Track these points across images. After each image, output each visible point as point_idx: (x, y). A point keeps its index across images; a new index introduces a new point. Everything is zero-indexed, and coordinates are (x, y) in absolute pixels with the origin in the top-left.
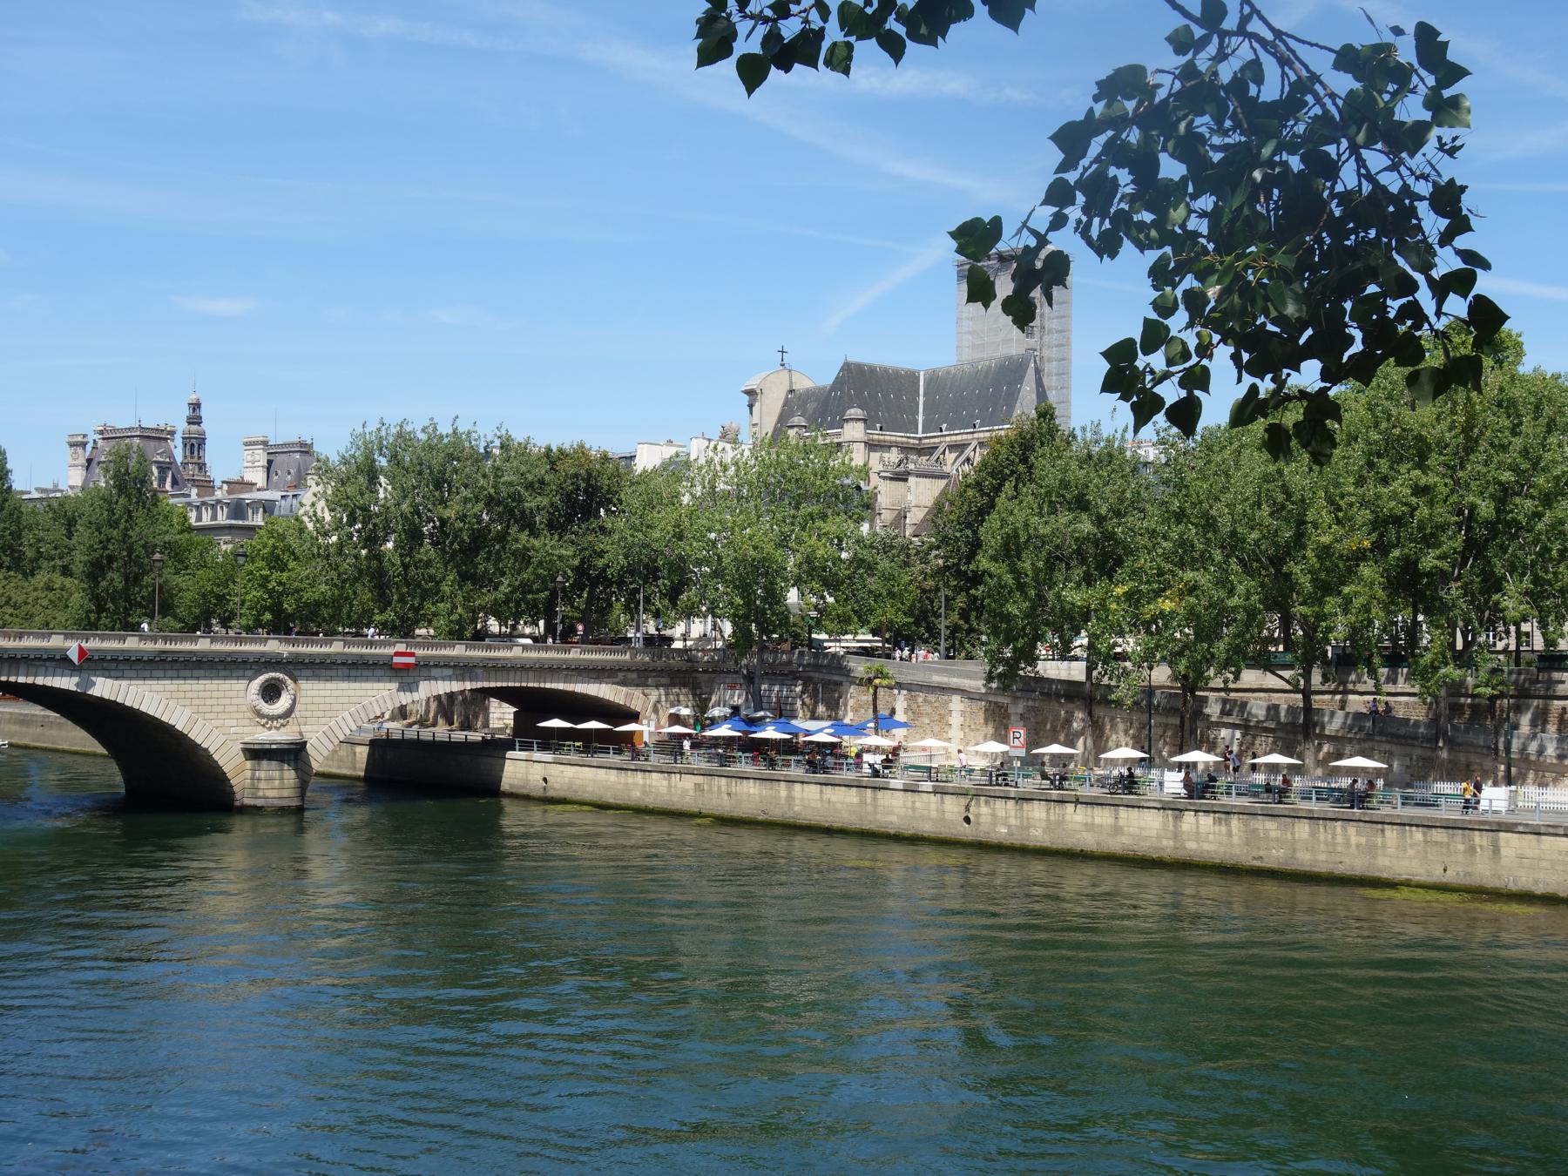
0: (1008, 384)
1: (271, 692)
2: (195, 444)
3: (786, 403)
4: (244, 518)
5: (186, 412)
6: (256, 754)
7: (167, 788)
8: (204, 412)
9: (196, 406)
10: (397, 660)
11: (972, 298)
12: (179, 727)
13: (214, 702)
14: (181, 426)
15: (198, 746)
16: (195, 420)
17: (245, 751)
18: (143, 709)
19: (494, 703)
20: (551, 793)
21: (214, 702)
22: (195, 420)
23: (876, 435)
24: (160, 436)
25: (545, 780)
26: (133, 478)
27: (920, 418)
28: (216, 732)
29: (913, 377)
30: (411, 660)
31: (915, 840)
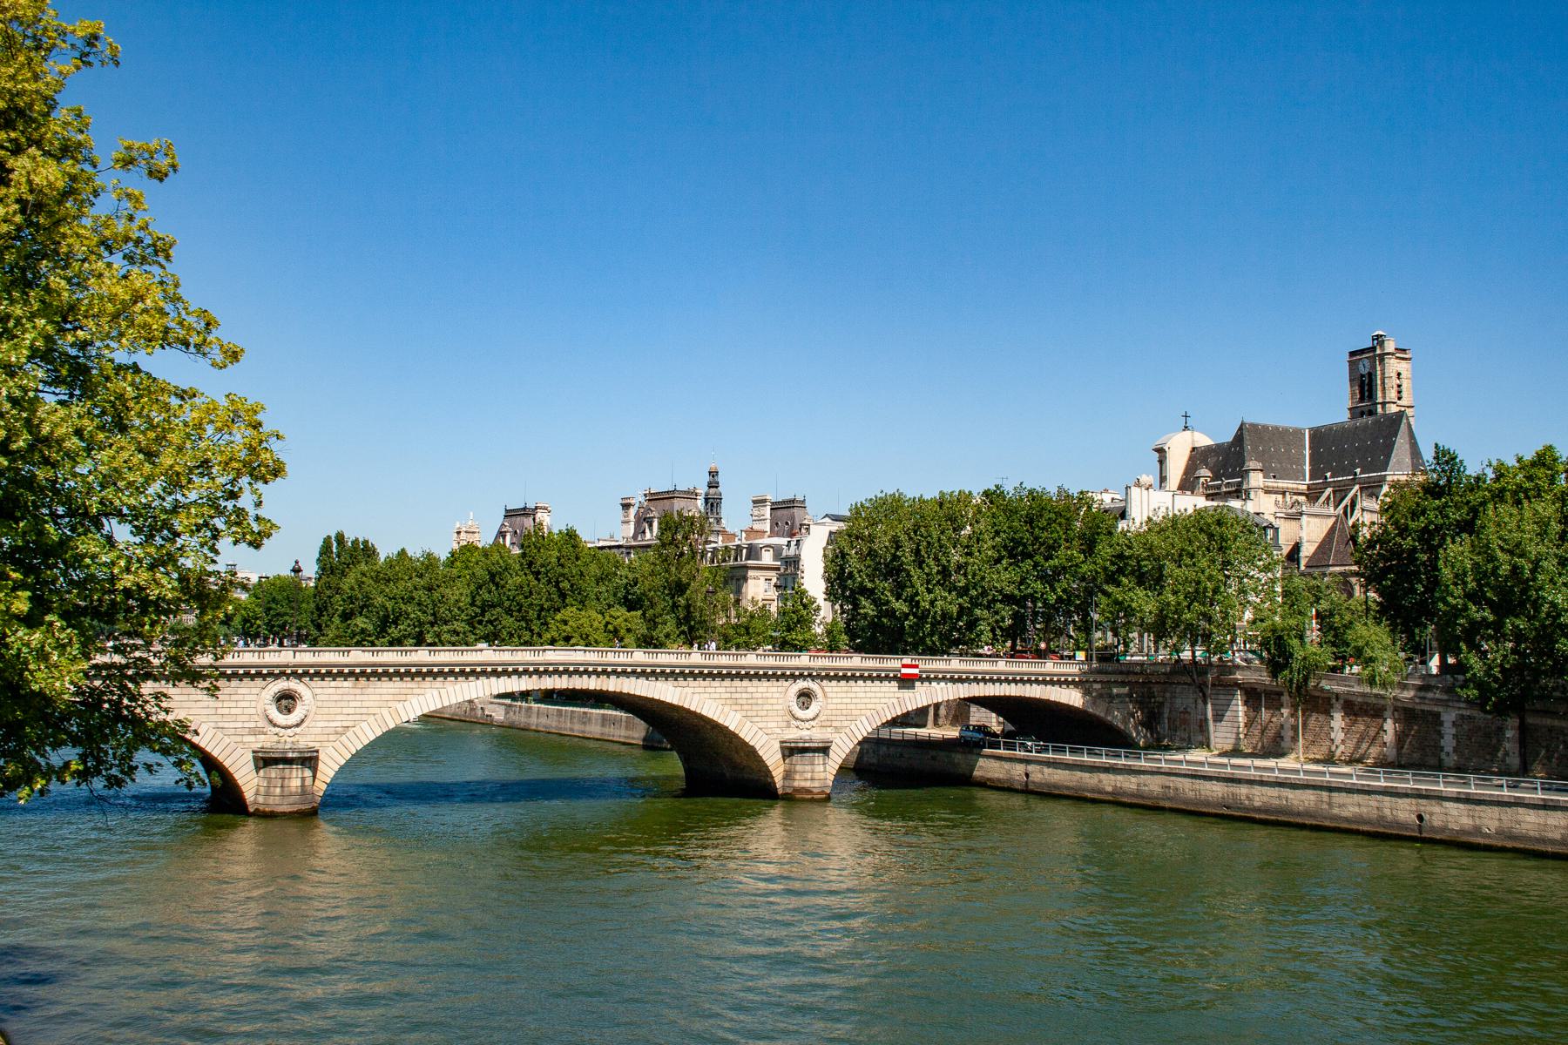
0: (1385, 438)
1: (286, 700)
2: (713, 503)
3: (1191, 458)
4: (758, 558)
5: (707, 478)
6: (265, 761)
7: (717, 774)
8: (720, 479)
9: (714, 474)
11: (161, 180)
14: (702, 490)
16: (713, 485)
17: (255, 759)
18: (704, 713)
19: (973, 708)
20: (1031, 787)
22: (713, 485)
24: (691, 495)
26: (676, 528)
27: (1307, 468)
28: (227, 740)
29: (1298, 433)
30: (916, 671)
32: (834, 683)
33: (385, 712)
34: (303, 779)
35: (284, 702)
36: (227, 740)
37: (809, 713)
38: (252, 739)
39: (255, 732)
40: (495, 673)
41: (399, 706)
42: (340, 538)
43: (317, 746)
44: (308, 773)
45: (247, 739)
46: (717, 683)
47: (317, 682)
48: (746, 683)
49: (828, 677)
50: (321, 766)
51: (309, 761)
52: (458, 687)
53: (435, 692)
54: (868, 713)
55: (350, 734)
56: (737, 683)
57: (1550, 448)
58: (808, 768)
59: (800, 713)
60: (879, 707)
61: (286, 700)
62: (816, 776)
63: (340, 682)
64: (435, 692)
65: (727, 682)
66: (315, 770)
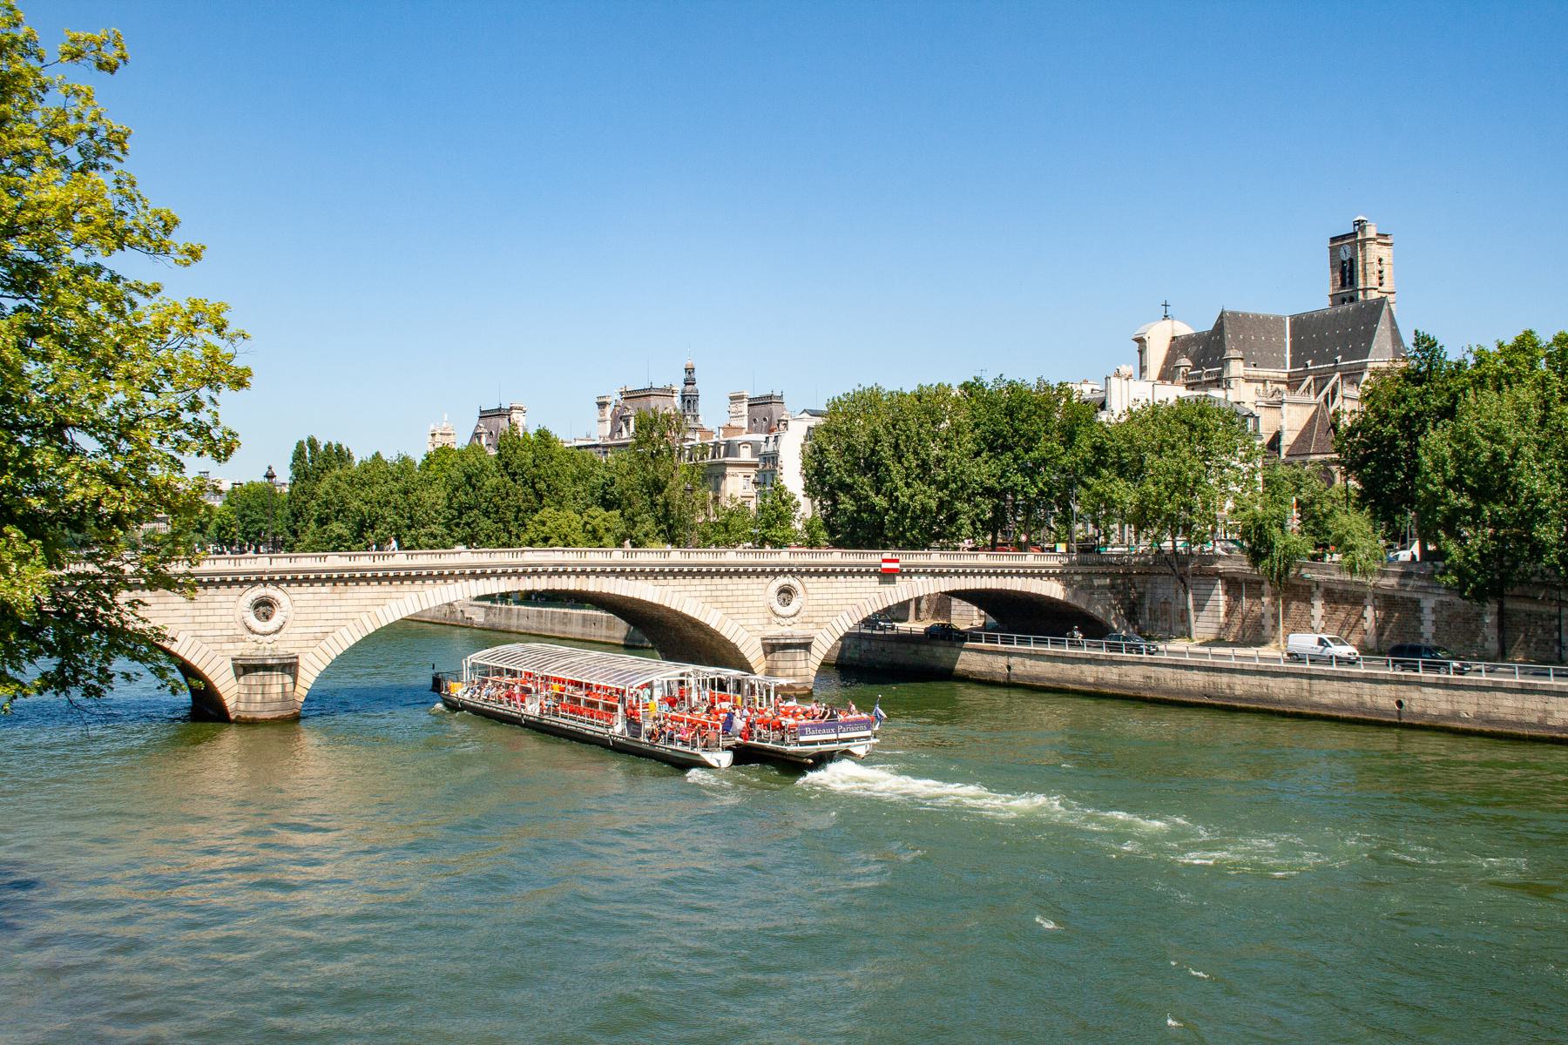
1: (264, 607)
2: (690, 400)
3: (1171, 348)
5: (684, 375)
9: (689, 371)
10: (885, 565)
12: (713, 626)
13: (224, 612)
14: (679, 387)
15: (727, 641)
16: (689, 382)
19: (955, 602)
20: (1013, 679)
21: (224, 612)
22: (689, 382)
23: (1252, 372)
25: (1400, 704)
26: (652, 428)
27: (1288, 356)
29: (1279, 321)
30: (896, 566)
31: (1228, 708)
32: (815, 579)
33: (364, 616)
34: (284, 685)
35: (262, 609)
36: (205, 648)
37: (271, 625)
38: (231, 646)
39: (234, 639)
40: (474, 576)
41: (378, 610)
42: (313, 444)
43: (296, 652)
44: (288, 679)
45: (225, 646)
46: (697, 581)
47: (294, 588)
48: (726, 580)
49: (808, 573)
50: (301, 672)
51: (289, 667)
52: (436, 590)
53: (414, 596)
54: (849, 608)
55: (329, 639)
56: (717, 580)
57: (1529, 333)
58: (789, 664)
59: (781, 610)
60: (860, 602)
61: (264, 607)
62: (798, 672)
63: (317, 588)
64: (414, 596)
65: (707, 580)
66: (295, 677)
